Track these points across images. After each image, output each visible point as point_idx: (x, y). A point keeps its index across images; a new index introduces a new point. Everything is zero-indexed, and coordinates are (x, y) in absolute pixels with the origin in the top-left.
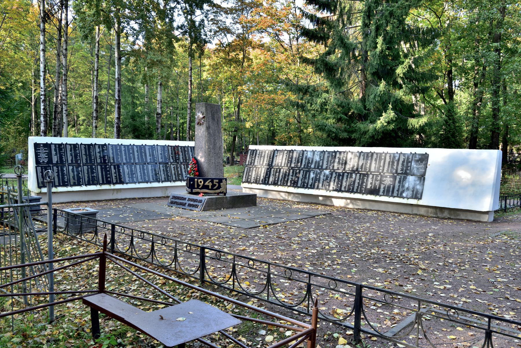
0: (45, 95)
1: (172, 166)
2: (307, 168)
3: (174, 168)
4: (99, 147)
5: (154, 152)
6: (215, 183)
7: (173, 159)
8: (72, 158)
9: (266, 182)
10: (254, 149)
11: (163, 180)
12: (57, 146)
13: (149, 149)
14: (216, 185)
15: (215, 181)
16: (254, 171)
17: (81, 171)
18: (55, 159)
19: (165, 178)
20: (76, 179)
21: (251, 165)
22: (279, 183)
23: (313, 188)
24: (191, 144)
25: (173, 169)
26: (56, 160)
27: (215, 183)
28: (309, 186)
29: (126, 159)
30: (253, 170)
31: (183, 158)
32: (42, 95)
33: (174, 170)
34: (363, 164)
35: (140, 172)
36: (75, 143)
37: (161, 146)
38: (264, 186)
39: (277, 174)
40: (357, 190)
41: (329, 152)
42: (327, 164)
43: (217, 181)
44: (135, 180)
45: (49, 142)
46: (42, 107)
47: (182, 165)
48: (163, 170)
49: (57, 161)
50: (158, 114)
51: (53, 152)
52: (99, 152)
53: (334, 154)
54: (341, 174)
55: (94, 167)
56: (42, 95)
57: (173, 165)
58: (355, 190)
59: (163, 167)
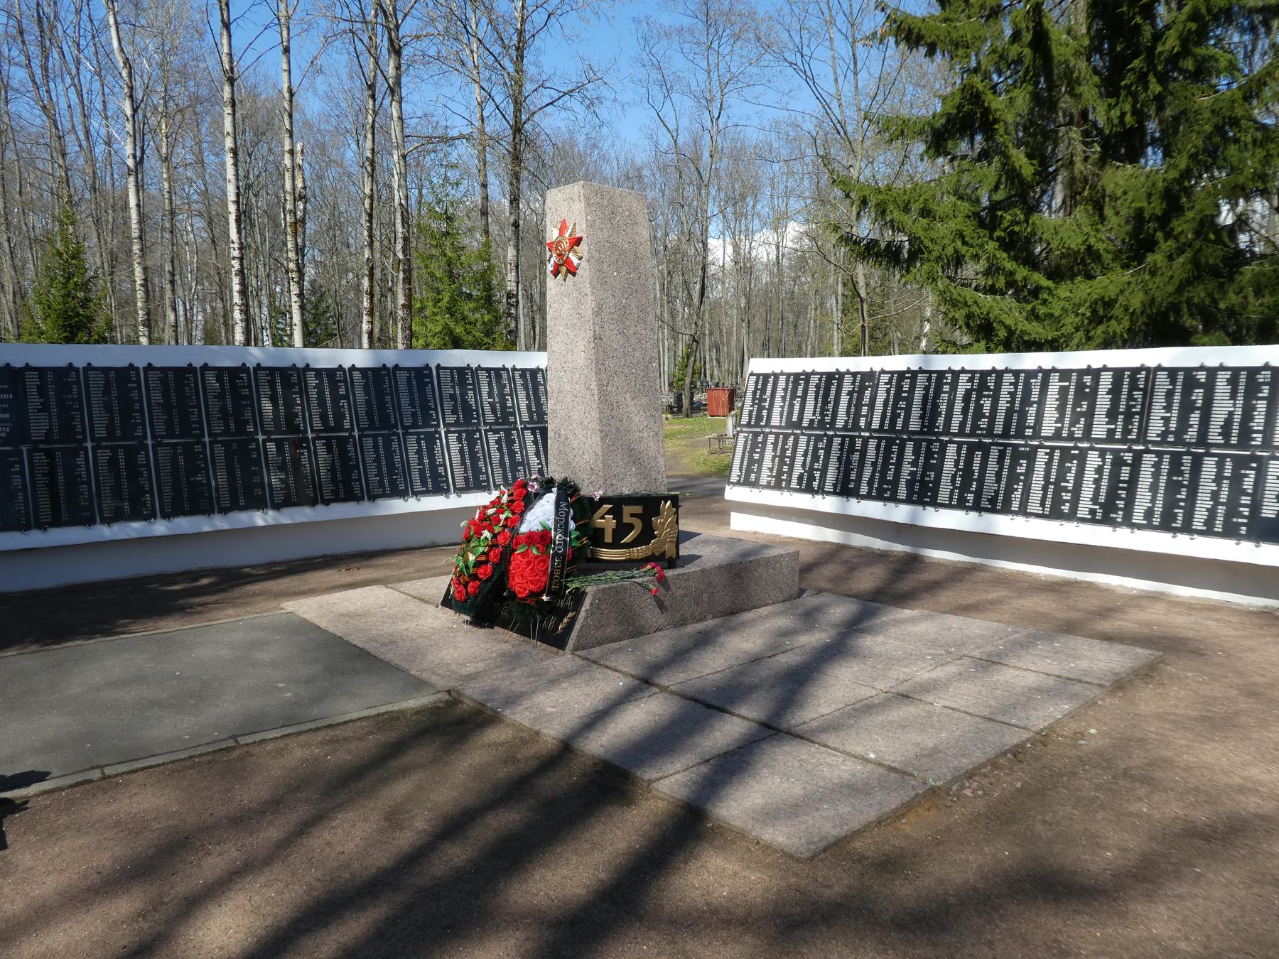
0: (241, 259)
1: (493, 438)
2: (972, 434)
3: (498, 442)
4: (219, 379)
5: (428, 389)
6: (627, 519)
7: (494, 411)
8: (111, 419)
9: (815, 484)
10: (769, 371)
11: (460, 484)
12: (50, 377)
13: (409, 379)
14: (630, 527)
15: (628, 510)
16: (769, 447)
17: (148, 466)
18: (39, 425)
19: (466, 479)
20: (126, 495)
21: (757, 425)
22: (864, 489)
23: (1006, 510)
24: (400, 346)
25: (493, 446)
26: (44, 428)
27: (627, 519)
28: (985, 504)
29: (324, 417)
30: (764, 443)
31: (529, 407)
32: (234, 258)
33: (500, 449)
34: (1231, 414)
35: (377, 460)
36: (124, 364)
37: (451, 369)
38: (1167, 536)
39: (856, 456)
40: (1210, 522)
41: (1065, 374)
42: (1060, 419)
43: (638, 509)
44: (357, 491)
45: (18, 364)
46: (236, 288)
47: (528, 434)
48: (461, 451)
49: (49, 434)
50: (509, 295)
51: (34, 400)
52: (221, 396)
53: (1088, 380)
54: (1128, 457)
55: (198, 448)
56: (234, 258)
57: (496, 432)
58: (1198, 524)
59: (459, 440)
